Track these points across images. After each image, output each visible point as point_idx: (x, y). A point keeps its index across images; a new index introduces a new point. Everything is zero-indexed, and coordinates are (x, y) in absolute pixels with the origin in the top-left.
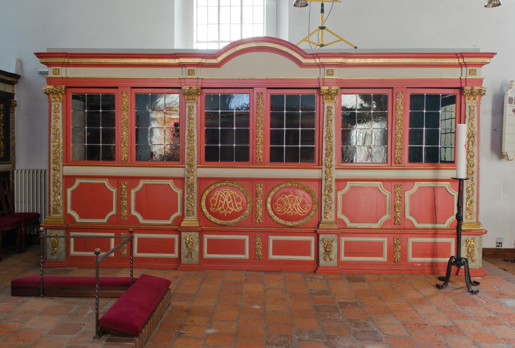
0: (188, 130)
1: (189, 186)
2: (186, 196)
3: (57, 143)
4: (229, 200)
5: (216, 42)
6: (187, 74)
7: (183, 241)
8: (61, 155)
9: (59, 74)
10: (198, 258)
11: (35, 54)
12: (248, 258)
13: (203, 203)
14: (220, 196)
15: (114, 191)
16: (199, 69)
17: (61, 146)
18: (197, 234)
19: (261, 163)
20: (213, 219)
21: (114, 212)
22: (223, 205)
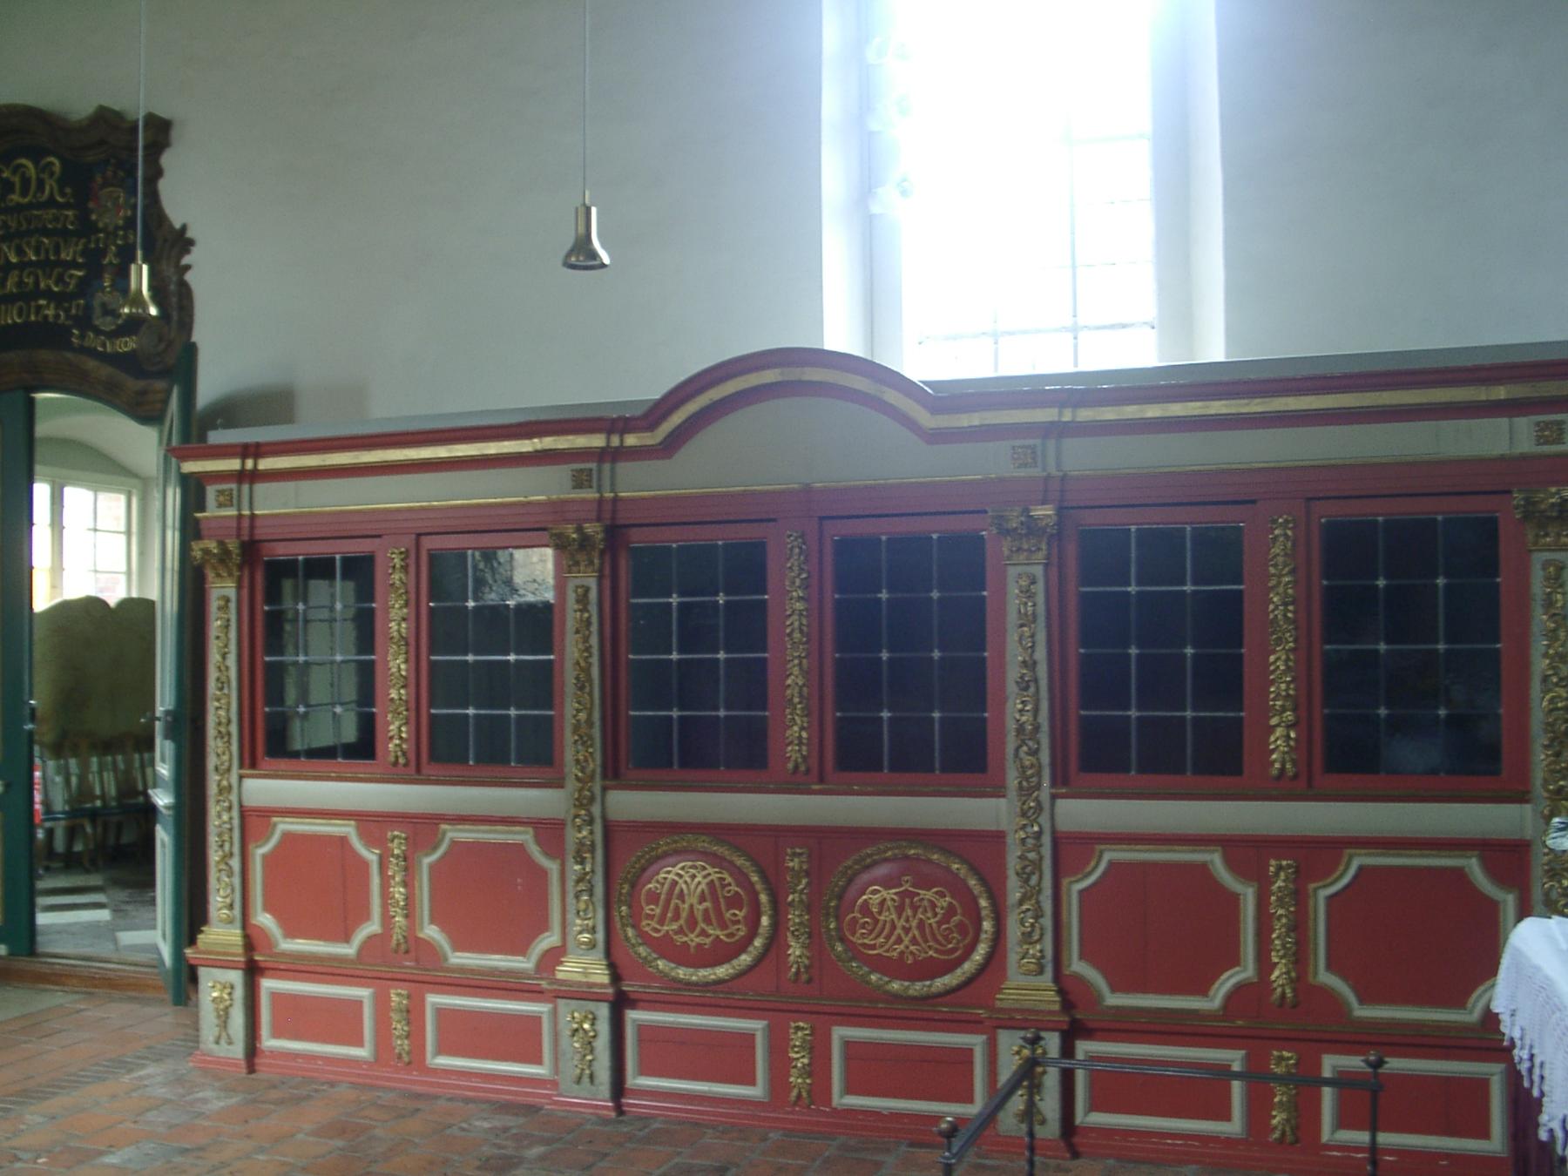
4: (702, 899)
5: (1066, 329)
9: (1538, 424)
14: (675, 883)
22: (684, 915)
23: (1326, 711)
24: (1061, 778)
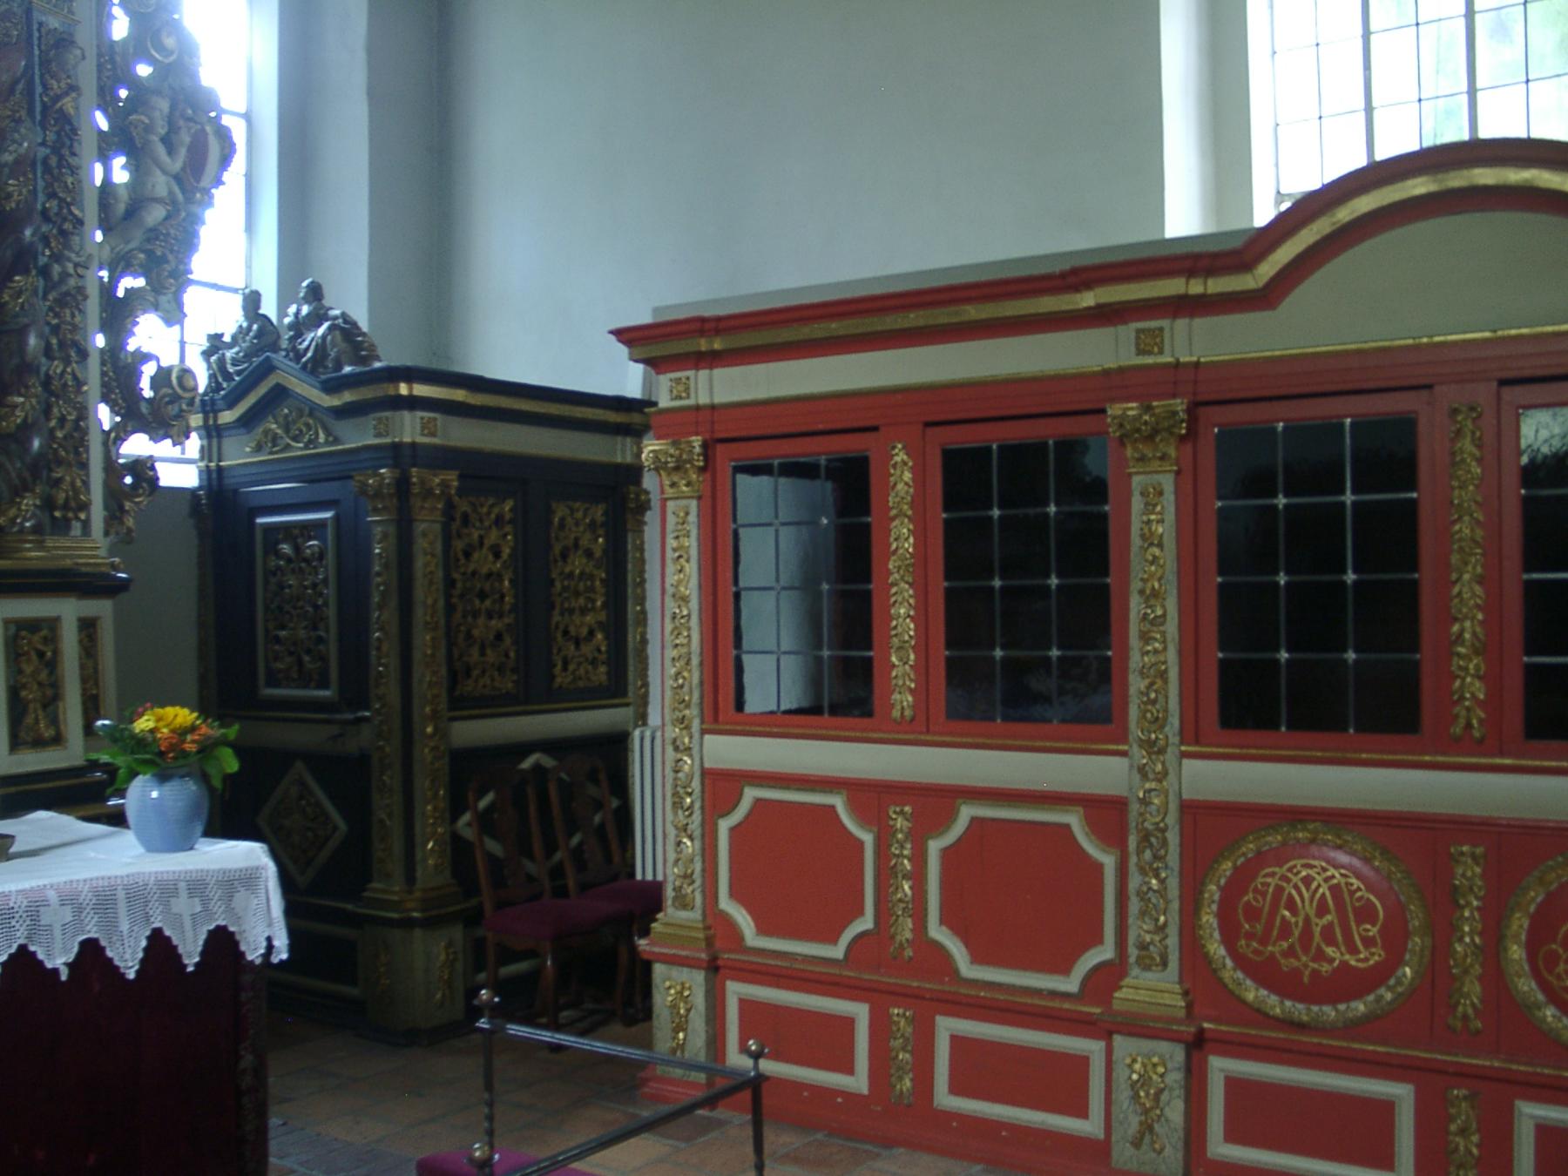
0: (1142, 592)
1: (1145, 838)
2: (1134, 882)
3: (684, 650)
4: (1322, 910)
6: (1133, 349)
7: (1120, 1073)
8: (696, 695)
9: (688, 397)
10: (1180, 1155)
11: (611, 332)
12: (865, 1091)
13: (1209, 918)
14: (1279, 890)
15: (867, 838)
16: (1181, 324)
17: (695, 661)
18: (1178, 1053)
19: (1463, 744)
20: (1252, 993)
21: (866, 923)
22: (1296, 933)
23: (1418, 656)
24: (1192, 733)
